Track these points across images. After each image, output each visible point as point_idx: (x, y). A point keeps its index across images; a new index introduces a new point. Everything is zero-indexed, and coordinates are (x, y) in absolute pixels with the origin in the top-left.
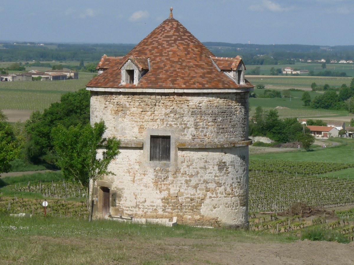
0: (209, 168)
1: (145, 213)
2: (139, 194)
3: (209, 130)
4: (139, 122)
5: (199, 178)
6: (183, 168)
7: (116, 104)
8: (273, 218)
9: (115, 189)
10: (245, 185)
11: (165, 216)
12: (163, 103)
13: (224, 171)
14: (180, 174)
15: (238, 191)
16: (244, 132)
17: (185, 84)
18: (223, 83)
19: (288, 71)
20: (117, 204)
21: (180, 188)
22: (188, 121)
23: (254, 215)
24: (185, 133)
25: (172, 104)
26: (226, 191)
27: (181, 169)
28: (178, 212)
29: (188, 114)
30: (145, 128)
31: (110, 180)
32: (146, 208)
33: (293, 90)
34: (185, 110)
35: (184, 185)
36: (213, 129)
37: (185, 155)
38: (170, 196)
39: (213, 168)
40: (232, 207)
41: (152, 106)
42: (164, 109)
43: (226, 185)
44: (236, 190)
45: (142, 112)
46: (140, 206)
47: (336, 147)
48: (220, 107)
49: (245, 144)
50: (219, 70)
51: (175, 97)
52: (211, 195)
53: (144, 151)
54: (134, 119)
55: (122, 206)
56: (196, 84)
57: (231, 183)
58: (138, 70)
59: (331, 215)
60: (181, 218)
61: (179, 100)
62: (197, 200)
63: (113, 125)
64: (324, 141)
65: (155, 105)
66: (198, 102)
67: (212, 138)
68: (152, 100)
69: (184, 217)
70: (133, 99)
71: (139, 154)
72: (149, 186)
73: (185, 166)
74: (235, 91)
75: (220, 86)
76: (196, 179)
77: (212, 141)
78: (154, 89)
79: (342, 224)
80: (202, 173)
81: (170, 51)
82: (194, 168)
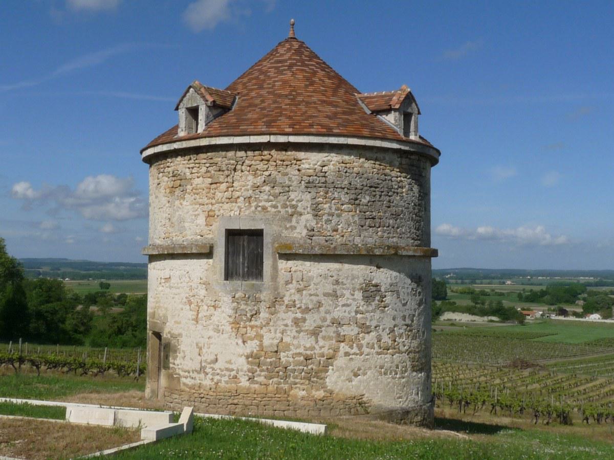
0: (343, 295)
1: (217, 384)
2: (206, 345)
3: (342, 219)
4: (207, 204)
5: (323, 314)
6: (288, 294)
7: (171, 175)
8: (499, 370)
9: (169, 336)
10: (424, 333)
11: (253, 391)
12: (250, 166)
13: (376, 302)
14: (284, 307)
15: (406, 343)
16: (418, 230)
17: (291, 126)
18: (373, 129)
19: (509, 282)
20: (171, 365)
21: (283, 334)
22: (299, 201)
23: (484, 367)
24: (294, 223)
25: (267, 166)
26: (380, 341)
27: (284, 296)
28: (279, 383)
29: (299, 187)
30: (216, 216)
31: (162, 318)
32: (218, 374)
33: (512, 292)
34: (293, 179)
35: (290, 328)
36: (351, 218)
37: (293, 269)
38: (262, 351)
39: (353, 295)
40: (393, 373)
41: (229, 172)
42: (250, 177)
43: (380, 331)
44: (401, 340)
45: (211, 184)
46: (208, 370)
47: (540, 323)
48: (365, 175)
49: (419, 251)
50: (369, 112)
51: (273, 152)
52: (348, 349)
53: (214, 260)
54: (198, 200)
55: (179, 369)
56: (315, 127)
57: (392, 327)
58: (205, 105)
59: (543, 368)
60: (286, 396)
61: (281, 158)
62: (318, 359)
63: (167, 215)
64: (532, 320)
65: (235, 170)
66: (318, 164)
67: (350, 236)
68: (229, 159)
69: (292, 392)
70: (196, 161)
71: (206, 267)
72: (223, 331)
73: (293, 291)
74: (395, 146)
75: (364, 132)
76: (316, 316)
77: (349, 241)
78: (229, 137)
79: (552, 375)
80: (329, 305)
81: (277, 81)
82: (311, 295)
